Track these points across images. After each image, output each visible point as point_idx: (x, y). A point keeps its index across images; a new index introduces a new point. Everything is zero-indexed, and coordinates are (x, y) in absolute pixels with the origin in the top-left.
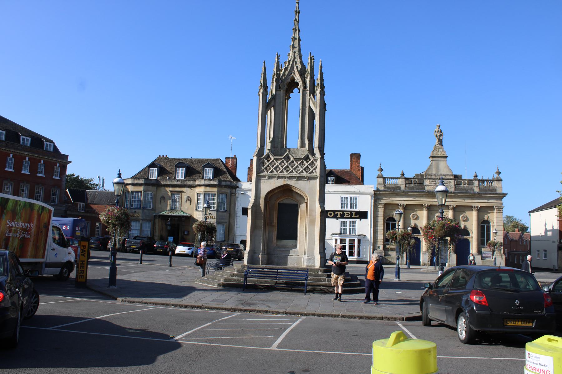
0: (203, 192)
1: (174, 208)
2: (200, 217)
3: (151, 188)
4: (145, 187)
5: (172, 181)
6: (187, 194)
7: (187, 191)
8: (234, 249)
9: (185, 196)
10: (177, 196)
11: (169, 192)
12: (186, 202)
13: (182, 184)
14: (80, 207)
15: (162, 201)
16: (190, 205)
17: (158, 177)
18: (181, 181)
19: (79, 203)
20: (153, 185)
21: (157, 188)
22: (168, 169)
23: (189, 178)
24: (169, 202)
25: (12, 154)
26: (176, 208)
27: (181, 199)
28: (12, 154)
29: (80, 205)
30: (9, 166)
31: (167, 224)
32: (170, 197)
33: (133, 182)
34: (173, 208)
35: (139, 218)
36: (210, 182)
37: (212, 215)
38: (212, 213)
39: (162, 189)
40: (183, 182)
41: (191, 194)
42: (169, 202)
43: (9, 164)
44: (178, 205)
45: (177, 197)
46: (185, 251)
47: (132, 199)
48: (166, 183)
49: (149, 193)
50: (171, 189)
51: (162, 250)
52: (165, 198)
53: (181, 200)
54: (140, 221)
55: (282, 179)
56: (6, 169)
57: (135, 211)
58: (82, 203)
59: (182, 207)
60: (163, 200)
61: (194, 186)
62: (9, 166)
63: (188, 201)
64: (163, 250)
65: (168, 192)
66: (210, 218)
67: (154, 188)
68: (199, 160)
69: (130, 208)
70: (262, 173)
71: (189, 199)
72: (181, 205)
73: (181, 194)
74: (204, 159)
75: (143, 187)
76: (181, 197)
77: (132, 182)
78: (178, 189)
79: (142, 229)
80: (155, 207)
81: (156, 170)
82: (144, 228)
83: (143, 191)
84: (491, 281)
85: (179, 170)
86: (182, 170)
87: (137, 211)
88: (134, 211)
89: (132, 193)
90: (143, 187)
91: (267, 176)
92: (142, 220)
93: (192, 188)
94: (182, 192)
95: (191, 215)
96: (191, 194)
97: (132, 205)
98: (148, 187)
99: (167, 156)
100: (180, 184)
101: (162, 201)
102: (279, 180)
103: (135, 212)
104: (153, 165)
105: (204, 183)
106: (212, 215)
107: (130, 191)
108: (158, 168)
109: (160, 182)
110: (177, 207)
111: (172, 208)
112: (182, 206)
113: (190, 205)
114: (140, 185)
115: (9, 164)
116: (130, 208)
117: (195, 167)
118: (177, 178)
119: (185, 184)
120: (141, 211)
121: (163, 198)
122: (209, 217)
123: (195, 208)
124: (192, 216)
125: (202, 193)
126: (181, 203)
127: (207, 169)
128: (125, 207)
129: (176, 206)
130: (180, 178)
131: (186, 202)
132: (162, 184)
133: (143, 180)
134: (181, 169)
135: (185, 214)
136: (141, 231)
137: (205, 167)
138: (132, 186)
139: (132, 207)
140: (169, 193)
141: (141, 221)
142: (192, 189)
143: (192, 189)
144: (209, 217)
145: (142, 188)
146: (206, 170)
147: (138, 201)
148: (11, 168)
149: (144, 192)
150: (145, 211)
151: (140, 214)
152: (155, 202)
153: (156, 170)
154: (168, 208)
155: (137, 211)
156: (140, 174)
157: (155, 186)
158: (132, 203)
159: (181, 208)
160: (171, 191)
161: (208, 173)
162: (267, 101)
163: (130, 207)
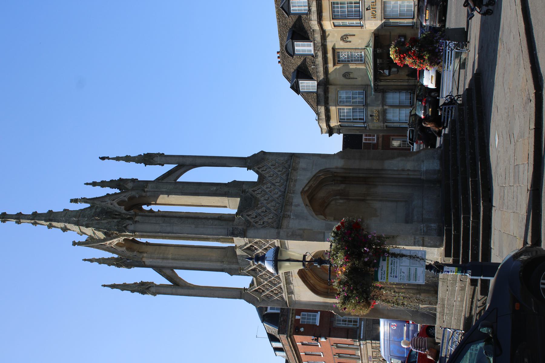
0: (332, 22)
1: (362, 58)
2: (373, 24)
3: (332, 95)
4: (330, 104)
5: (318, 64)
6: (336, 41)
7: (332, 42)
8: (427, 7)
9: (341, 44)
10: (342, 55)
11: (335, 67)
12: (350, 42)
13: (321, 49)
14: (369, 140)
15: (351, 76)
16: (354, 35)
17: (313, 79)
18: (316, 51)
19: (364, 141)
20: (326, 91)
21: (331, 85)
22: (299, 63)
23: (310, 35)
24: (352, 66)
25: (296, 316)
26: (362, 55)
27: (346, 50)
28: (296, 316)
29: (366, 139)
30: (313, 319)
31: (387, 74)
32: (343, 66)
33: (324, 120)
34: (361, 60)
35: (380, 110)
36: (313, 12)
37: (369, 6)
38: (366, 7)
39: (331, 77)
40: (318, 49)
41: (336, 35)
42: (352, 66)
43: (310, 319)
44: (356, 54)
45: (344, 55)
46: (432, 76)
47: (350, 119)
48: (322, 72)
49: (340, 101)
50: (330, 65)
51: (430, 109)
52: (347, 72)
53: (348, 50)
54: (386, 109)
55: (291, 278)
56: (318, 324)
57: (369, 116)
58: (364, 137)
59: (360, 48)
60: (349, 74)
61: (323, 32)
62: (313, 319)
63: (349, 40)
64: (430, 108)
65: (336, 69)
66: (375, 8)
67: (332, 89)
68: (280, 34)
69: (366, 122)
70: (285, 299)
71: (344, 38)
72: (355, 49)
73: (337, 51)
74: (276, 7)
75: (330, 107)
76: (342, 50)
77: (325, 123)
78: (330, 55)
79: (397, 104)
80: (362, 85)
81: (302, 83)
82: (397, 102)
83: (337, 107)
84: (449, 41)
85: (299, 51)
86: (298, 46)
87: (369, 113)
88: (370, 118)
89: (341, 120)
90: (330, 107)
91: (289, 296)
92: (383, 106)
93: (327, 35)
94: (334, 49)
95: (373, 33)
96: (336, 35)
97: (360, 119)
98: (330, 98)
99: (278, 52)
100: (321, 52)
101: (351, 76)
102: (292, 282)
103: (371, 116)
104: (296, 88)
105: (315, 20)
106: (369, 6)
107: (339, 124)
108: (298, 79)
109: (320, 81)
110: (359, 53)
111: (361, 60)
112: (357, 48)
113: (354, 35)
114: (327, 111)
115: (310, 319)
116: (366, 122)
117: (290, 21)
118: (313, 52)
119: (320, 44)
120: (370, 108)
121: (346, 76)
122: (374, 11)
123: (359, 29)
124: (373, 31)
125: (333, 22)
126: (353, 49)
127: (292, 8)
128: (363, 121)
129: (358, 55)
130: (312, 48)
131: (350, 42)
132: (324, 78)
133: (319, 107)
134: (296, 48)
135: (372, 44)
136: (400, 106)
137: (288, 13)
138: (331, 121)
139: (364, 120)
140: (338, 67)
141: (385, 107)
142: (329, 35)
143: (327, 34)
144: (374, 11)
145: (333, 109)
146: (293, 10)
147: (353, 111)
148: (315, 316)
149: (340, 106)
150: (368, 101)
151: (375, 109)
152: (353, 87)
153: (302, 83)
154: (363, 67)
155: (369, 113)
156: (312, 103)
157: (328, 88)
158: (357, 119)
159: (362, 49)
160: (334, 65)
161: (299, 6)
162: (171, 284)
163: (364, 122)
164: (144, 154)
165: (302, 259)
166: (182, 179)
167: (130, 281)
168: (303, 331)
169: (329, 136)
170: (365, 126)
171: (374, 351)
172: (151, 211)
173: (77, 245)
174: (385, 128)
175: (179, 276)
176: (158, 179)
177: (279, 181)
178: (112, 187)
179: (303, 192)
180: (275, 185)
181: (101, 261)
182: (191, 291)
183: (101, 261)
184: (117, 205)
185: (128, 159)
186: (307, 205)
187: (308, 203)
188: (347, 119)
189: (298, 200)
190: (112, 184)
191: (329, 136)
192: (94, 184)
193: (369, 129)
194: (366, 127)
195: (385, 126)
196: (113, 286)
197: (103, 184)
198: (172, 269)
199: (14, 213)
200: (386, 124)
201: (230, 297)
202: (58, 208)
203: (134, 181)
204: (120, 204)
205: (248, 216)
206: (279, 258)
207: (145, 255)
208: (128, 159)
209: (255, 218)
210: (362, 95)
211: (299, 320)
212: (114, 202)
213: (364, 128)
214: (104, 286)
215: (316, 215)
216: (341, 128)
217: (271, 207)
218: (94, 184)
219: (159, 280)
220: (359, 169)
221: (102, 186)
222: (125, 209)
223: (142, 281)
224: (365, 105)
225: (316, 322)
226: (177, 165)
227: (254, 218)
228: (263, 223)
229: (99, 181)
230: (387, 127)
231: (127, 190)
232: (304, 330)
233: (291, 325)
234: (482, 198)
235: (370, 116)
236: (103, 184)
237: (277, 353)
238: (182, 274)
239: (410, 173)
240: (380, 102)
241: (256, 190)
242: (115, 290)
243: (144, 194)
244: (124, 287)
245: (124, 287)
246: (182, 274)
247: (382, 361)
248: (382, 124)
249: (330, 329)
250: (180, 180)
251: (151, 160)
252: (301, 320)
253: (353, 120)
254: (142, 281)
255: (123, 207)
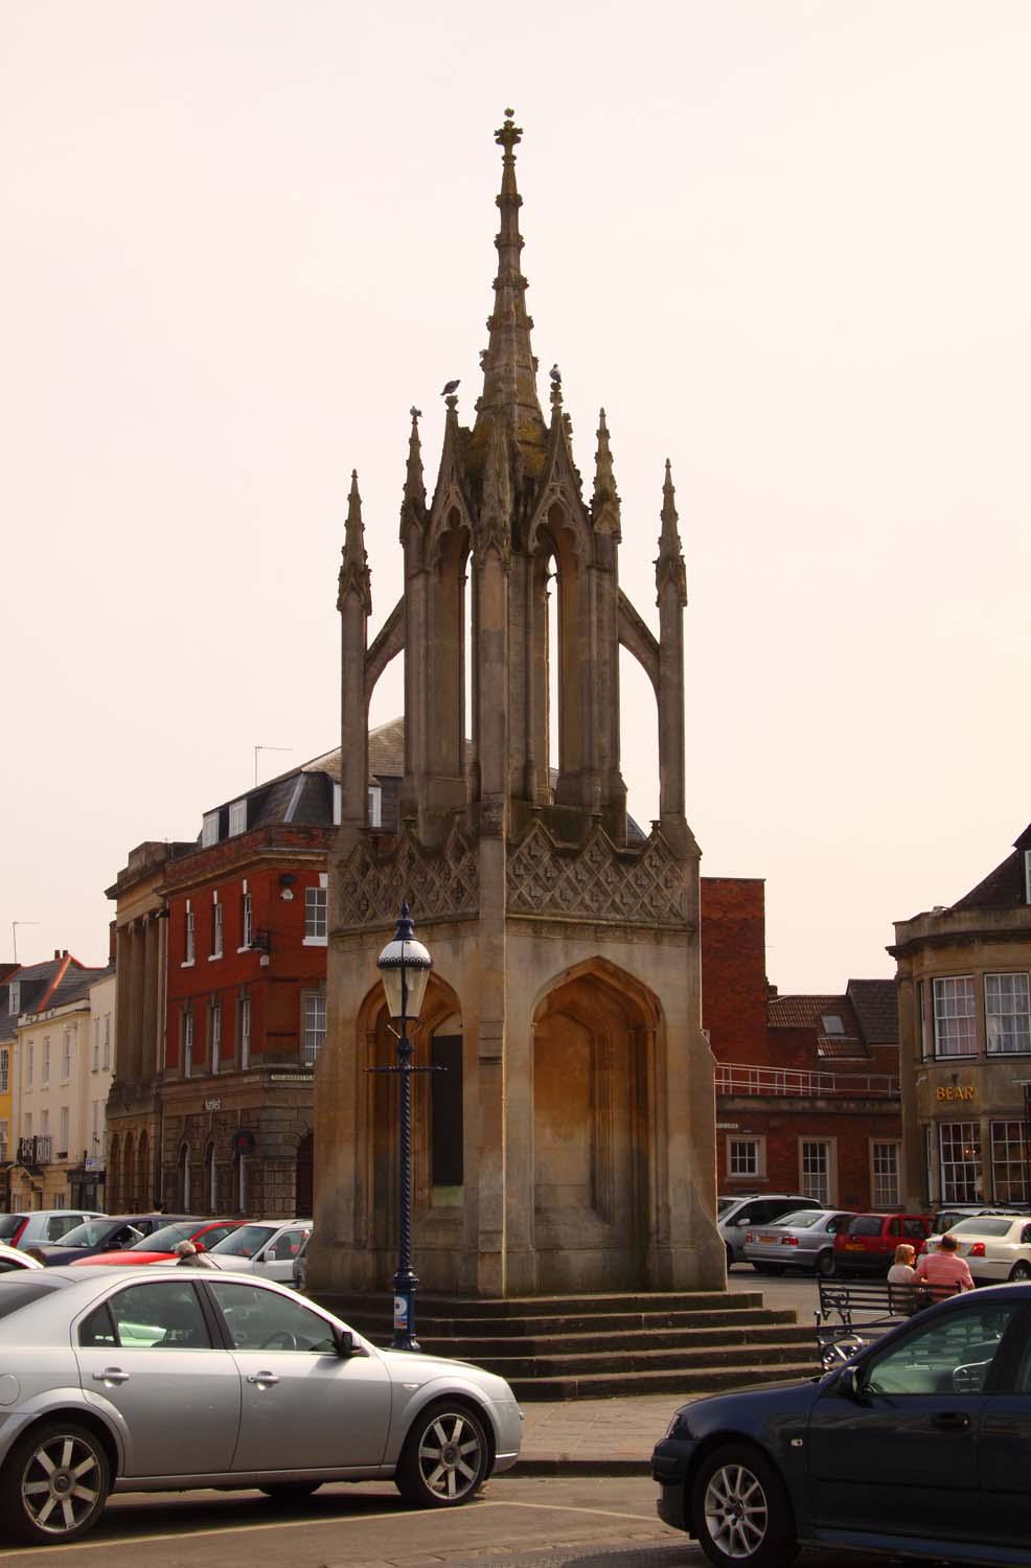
33: (935, 933)
87: (961, 1071)
88: (948, 1073)
103: (955, 1077)
155: (961, 1071)
164: (683, 557)
165: (407, 1014)
166: (624, 654)
167: (369, 540)
168: (282, 898)
169: (887, 948)
170: (925, 1060)
171: (235, 1117)
172: (546, 577)
173: (448, 408)
174: (920, 1122)
175: (389, 664)
176: (623, 599)
177: (625, 901)
178: (597, 481)
179: (600, 962)
180: (614, 893)
181: (414, 465)
182: (352, 695)
183: (414, 465)
184: (550, 502)
185: (669, 516)
186: (568, 974)
187: (576, 974)
188: (940, 1002)
189: (581, 952)
190: (605, 482)
191: (887, 948)
192: (603, 434)
193: (917, 1072)
194: (922, 1063)
195: (926, 1121)
196: (354, 499)
197: (604, 457)
198: (406, 645)
199: (524, 228)
200: (933, 1123)
201: (363, 720)
202: (541, 343)
203: (616, 536)
204: (555, 511)
205: (535, 837)
206: (407, 969)
207: (433, 579)
208: (669, 516)
209: (529, 854)
210: (1020, 1046)
211: (317, 884)
212: (559, 495)
213: (917, 1056)
214: (355, 476)
215: (548, 996)
216: (915, 983)
217: (558, 891)
218: (603, 434)
219: (375, 626)
220: (665, 1091)
221: (598, 457)
222: (541, 526)
223: (370, 571)
224: (988, 1057)
225: (313, 935)
226: (658, 641)
227: (515, 871)
228: (518, 876)
229: (612, 445)
230: (926, 1126)
231: (591, 521)
232: (287, 901)
233: (300, 860)
234: (442, 1323)
235: (954, 1073)
236: (604, 457)
237: (216, 817)
238: (395, 670)
239: (662, 1214)
240: (1000, 1103)
241: (599, 849)
242: (347, 505)
243: (582, 567)
244: (354, 525)
245: (354, 525)
246: (395, 670)
247: (207, 1140)
248: (932, 1111)
249: (295, 980)
250: (623, 651)
251: (667, 578)
252: (316, 889)
253: (940, 1021)
254: (370, 571)
255: (546, 519)
